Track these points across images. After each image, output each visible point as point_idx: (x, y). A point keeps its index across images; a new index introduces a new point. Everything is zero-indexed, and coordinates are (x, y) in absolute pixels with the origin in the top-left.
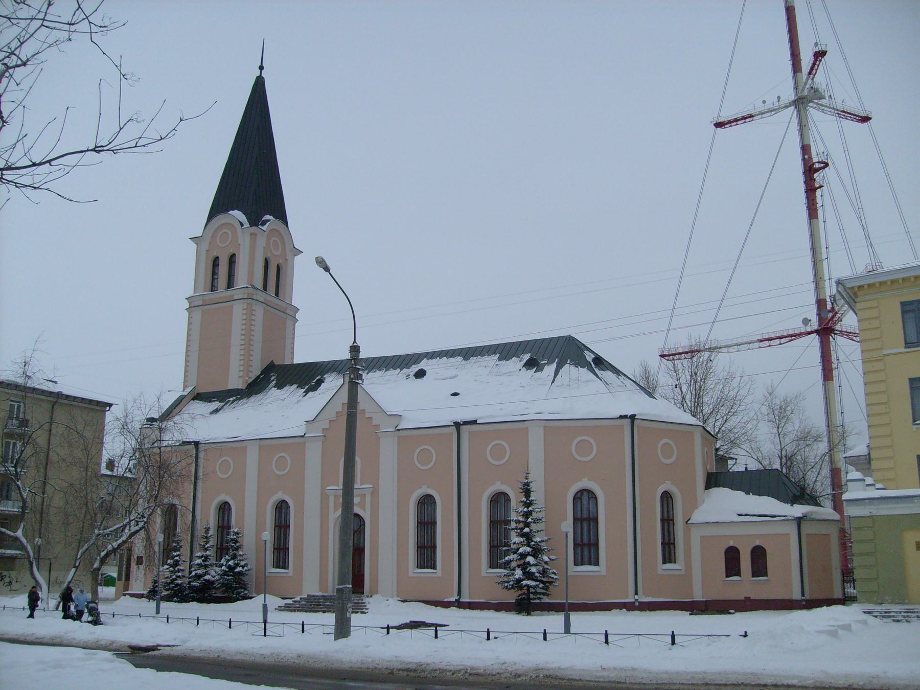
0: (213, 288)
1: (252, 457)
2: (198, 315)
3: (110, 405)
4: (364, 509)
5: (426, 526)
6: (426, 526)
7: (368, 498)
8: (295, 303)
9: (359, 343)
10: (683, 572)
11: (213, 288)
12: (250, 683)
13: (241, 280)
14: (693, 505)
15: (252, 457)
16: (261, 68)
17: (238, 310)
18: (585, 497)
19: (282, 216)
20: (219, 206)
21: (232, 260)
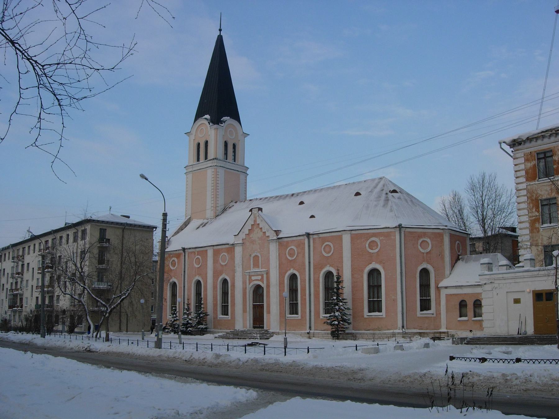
0: (198, 160)
1: (346, 240)
2: (190, 176)
3: (156, 228)
4: (263, 282)
5: (293, 291)
6: (293, 291)
7: (265, 276)
8: (246, 165)
9: (167, 211)
10: (435, 315)
11: (198, 160)
12: (83, 362)
13: (211, 155)
14: (441, 276)
15: (346, 240)
16: (220, 30)
17: (210, 173)
18: (375, 274)
19: (236, 116)
20: (199, 115)
21: (206, 143)
